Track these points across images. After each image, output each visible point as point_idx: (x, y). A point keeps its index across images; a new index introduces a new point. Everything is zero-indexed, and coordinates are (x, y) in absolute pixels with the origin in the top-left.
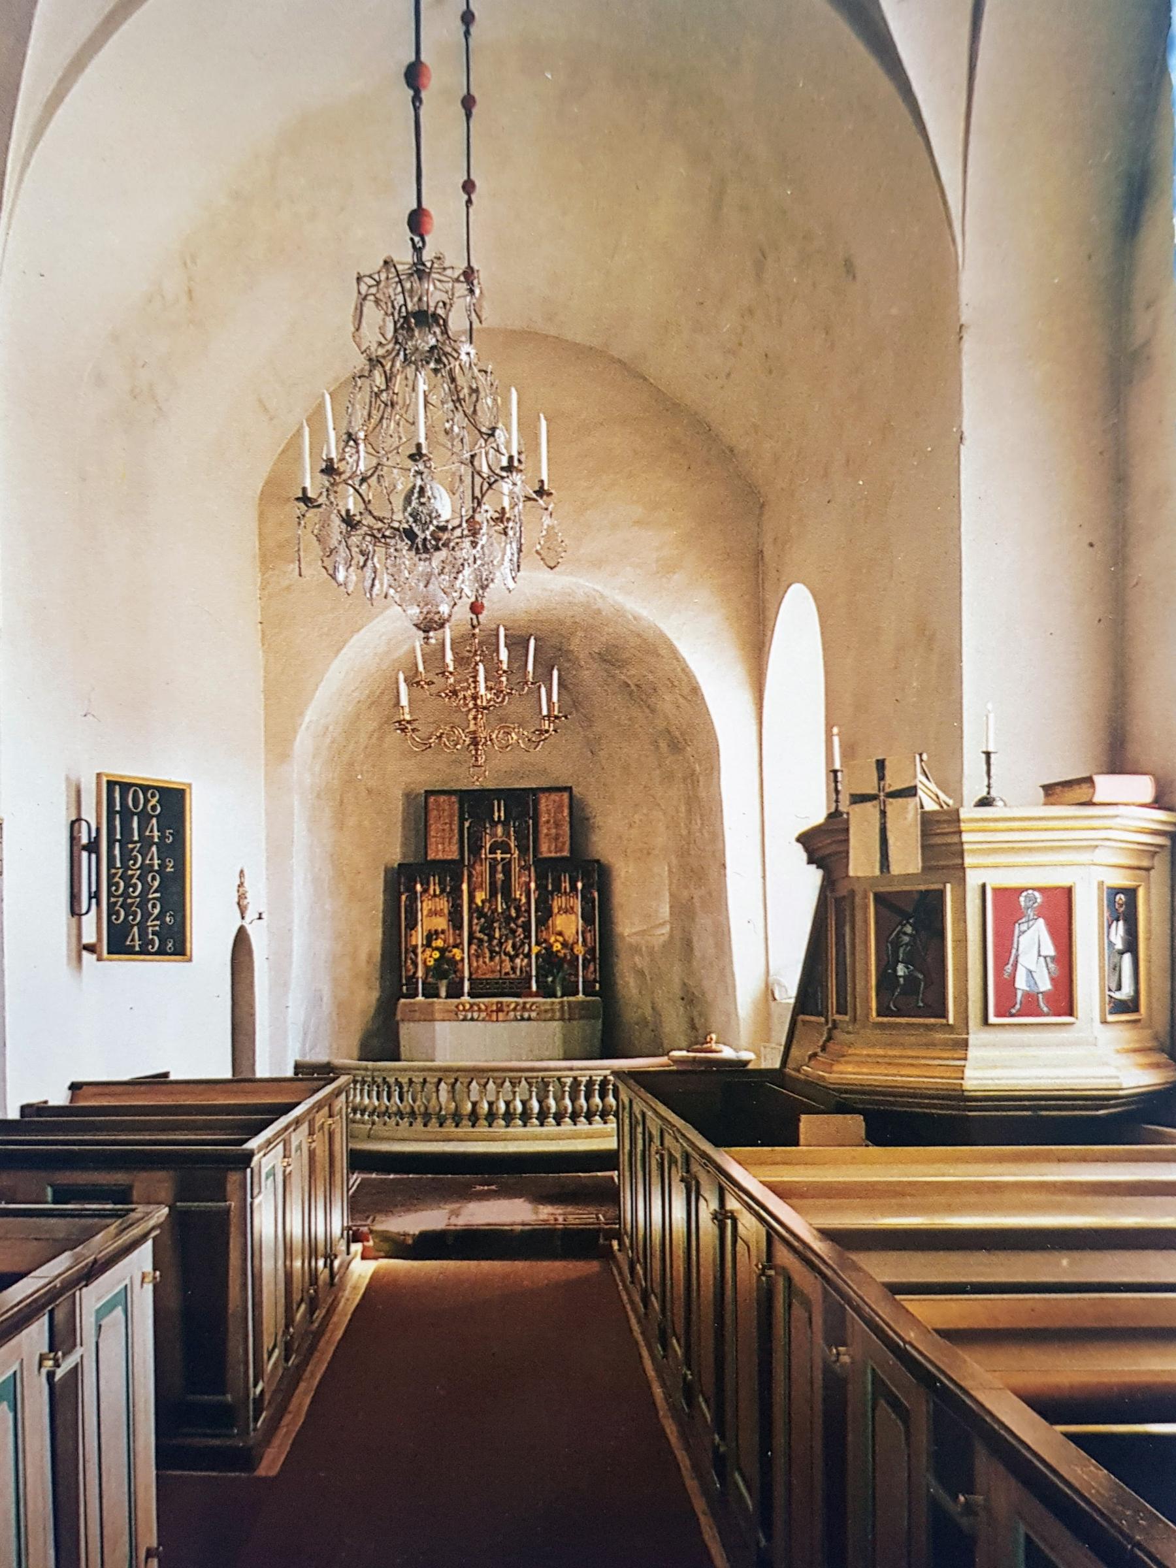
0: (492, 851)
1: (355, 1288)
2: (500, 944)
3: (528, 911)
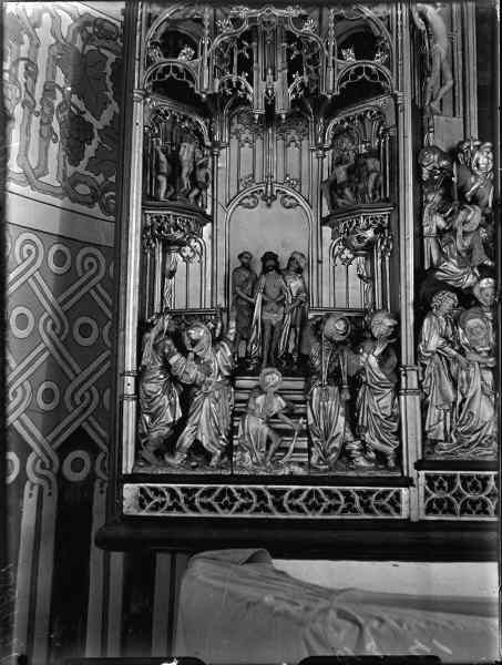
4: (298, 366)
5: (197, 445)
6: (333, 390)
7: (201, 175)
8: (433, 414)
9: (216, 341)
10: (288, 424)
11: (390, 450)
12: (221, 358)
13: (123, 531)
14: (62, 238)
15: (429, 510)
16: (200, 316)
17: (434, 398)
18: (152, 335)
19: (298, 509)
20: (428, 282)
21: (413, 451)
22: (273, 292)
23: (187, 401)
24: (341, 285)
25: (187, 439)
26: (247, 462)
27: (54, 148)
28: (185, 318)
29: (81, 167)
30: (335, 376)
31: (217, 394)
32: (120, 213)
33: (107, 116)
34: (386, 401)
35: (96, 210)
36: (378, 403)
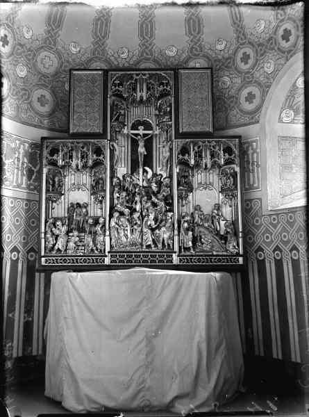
0: (134, 127)
1: (286, 168)
2: (142, 217)
3: (171, 187)
4: (81, 230)
5: (58, 249)
6: (90, 235)
7: (61, 183)
8: (113, 241)
9: (63, 225)
10: (79, 244)
11: (103, 249)
12: (64, 229)
13: (41, 268)
14: (27, 200)
15: (111, 262)
16: (61, 219)
17: (113, 237)
18: (48, 224)
19: (216, 262)
20: (112, 208)
21: (108, 249)
22: (78, 212)
23: (56, 239)
24: (95, 211)
25: (56, 248)
26: (70, 252)
27: (25, 178)
28: (56, 219)
29: (31, 182)
30: (90, 233)
32: (40, 191)
33: (38, 167)
34: (102, 238)
35: (36, 192)
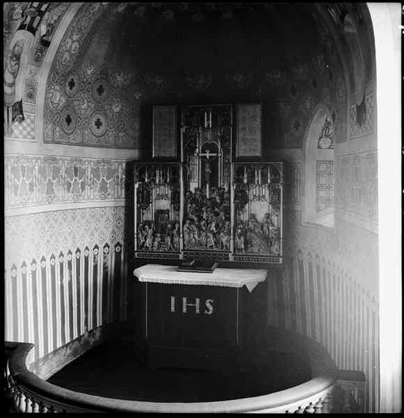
21: (181, 247)
27: (123, 190)
31: (86, 96)
36: (176, 240)
